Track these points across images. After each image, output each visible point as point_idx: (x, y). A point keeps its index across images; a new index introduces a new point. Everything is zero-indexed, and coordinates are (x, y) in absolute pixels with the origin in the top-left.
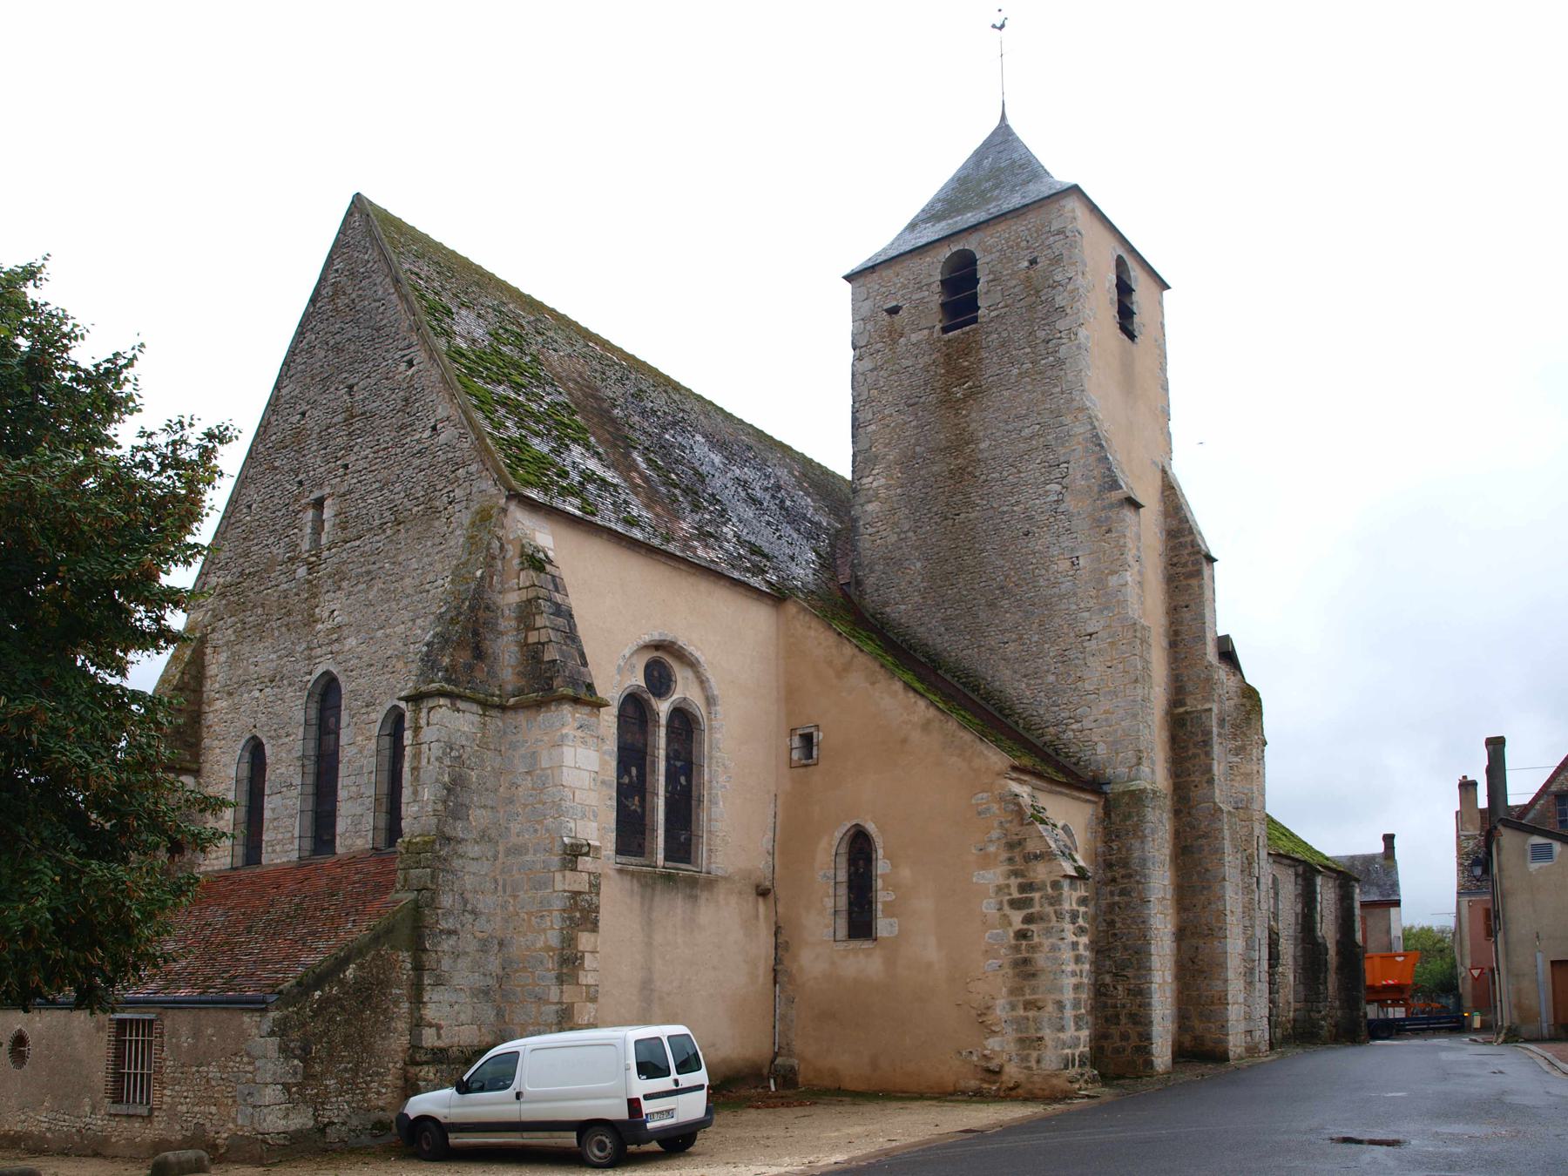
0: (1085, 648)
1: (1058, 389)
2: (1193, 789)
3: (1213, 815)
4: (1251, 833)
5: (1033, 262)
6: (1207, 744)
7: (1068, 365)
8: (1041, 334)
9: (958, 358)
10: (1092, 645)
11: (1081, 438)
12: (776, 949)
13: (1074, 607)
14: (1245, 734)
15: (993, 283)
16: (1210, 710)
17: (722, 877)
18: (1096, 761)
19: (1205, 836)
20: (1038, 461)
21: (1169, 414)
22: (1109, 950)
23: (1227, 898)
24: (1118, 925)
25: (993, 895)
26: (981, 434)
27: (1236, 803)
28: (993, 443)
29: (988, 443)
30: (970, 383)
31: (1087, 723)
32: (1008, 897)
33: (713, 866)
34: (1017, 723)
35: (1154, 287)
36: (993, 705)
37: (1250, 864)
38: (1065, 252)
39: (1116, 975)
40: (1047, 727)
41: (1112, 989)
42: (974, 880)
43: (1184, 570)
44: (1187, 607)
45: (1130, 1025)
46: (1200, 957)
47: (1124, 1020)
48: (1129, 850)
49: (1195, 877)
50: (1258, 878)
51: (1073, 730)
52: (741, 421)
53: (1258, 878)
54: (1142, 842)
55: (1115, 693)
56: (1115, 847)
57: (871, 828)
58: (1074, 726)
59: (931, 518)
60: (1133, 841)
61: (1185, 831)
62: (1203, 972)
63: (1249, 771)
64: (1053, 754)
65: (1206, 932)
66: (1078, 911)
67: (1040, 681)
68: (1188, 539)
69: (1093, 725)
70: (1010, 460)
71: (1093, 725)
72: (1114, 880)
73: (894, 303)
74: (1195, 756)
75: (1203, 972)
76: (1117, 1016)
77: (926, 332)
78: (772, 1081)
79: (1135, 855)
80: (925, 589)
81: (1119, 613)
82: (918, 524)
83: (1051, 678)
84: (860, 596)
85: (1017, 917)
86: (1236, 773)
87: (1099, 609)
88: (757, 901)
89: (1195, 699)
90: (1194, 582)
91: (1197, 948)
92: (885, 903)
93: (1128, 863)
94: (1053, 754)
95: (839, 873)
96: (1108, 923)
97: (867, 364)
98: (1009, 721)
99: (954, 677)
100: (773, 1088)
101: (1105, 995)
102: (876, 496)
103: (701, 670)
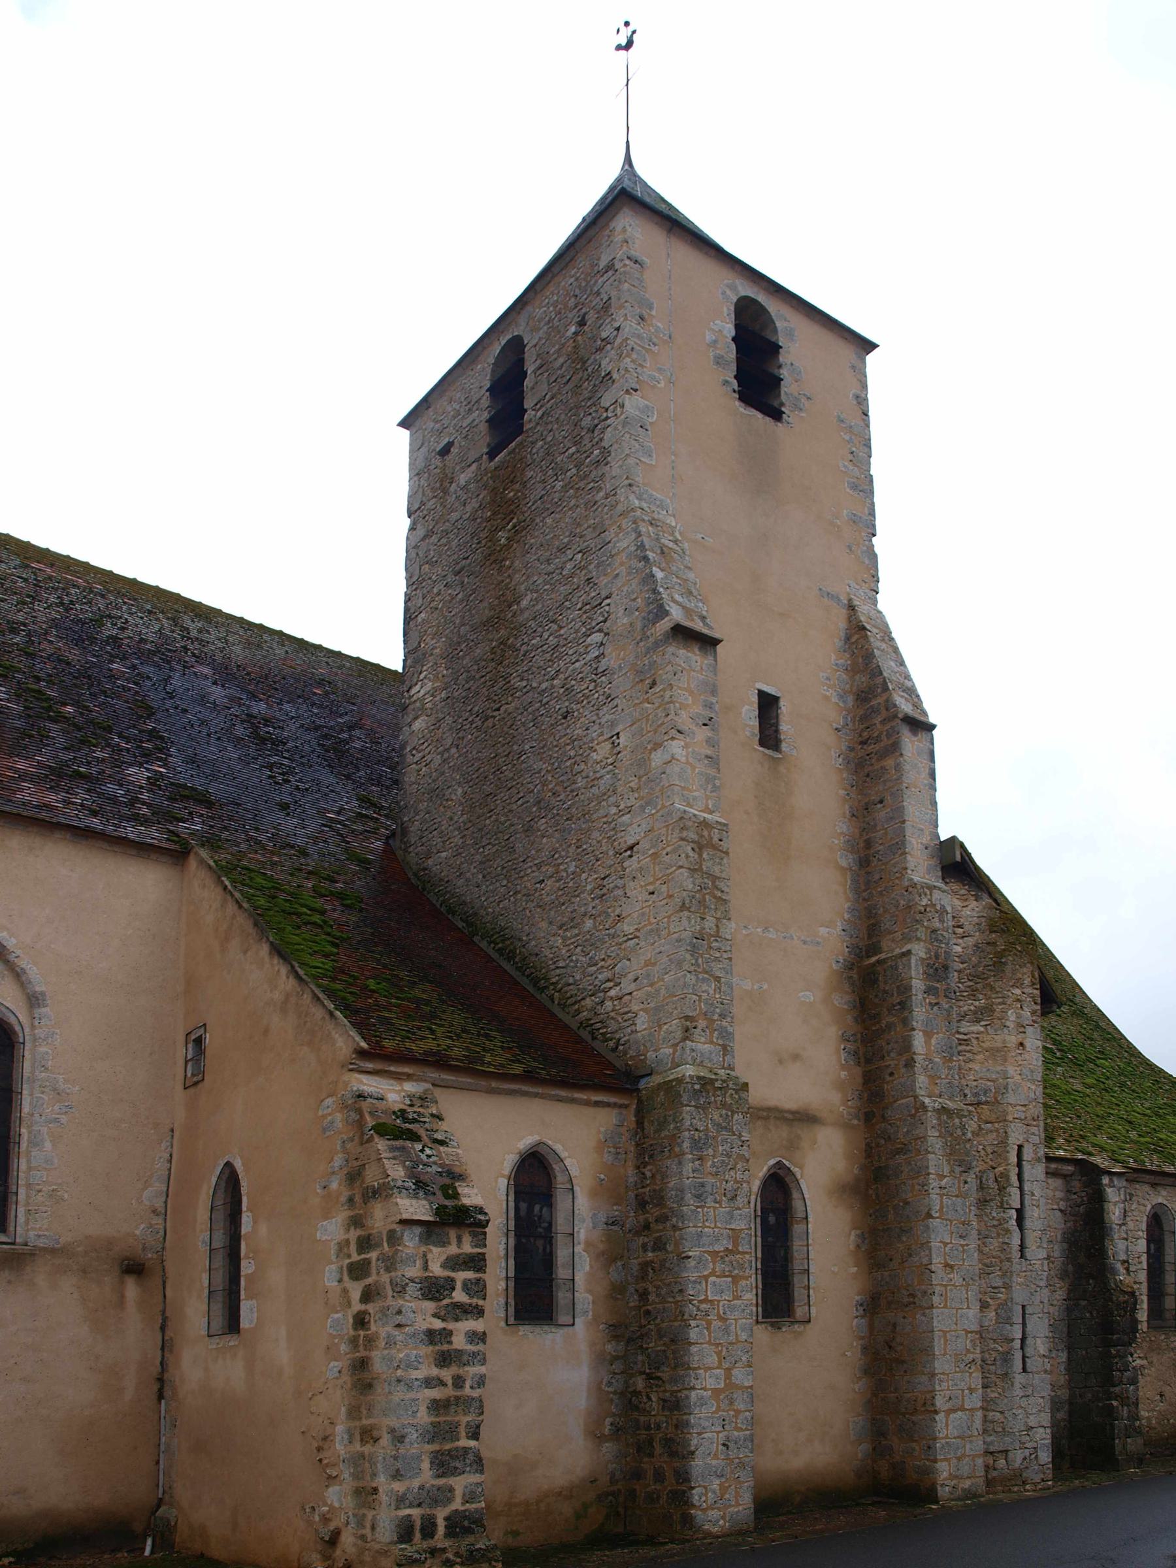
0: (624, 869)
1: (602, 494)
2: (888, 1078)
3: (913, 1116)
4: (1004, 1143)
5: (582, 323)
6: (904, 1005)
7: (613, 454)
8: (587, 422)
9: (505, 490)
10: (632, 864)
11: (624, 555)
12: (163, 1349)
13: (614, 810)
14: (992, 988)
15: (540, 372)
16: (909, 952)
17: (44, 1249)
18: (637, 1042)
19: (904, 1149)
20: (579, 606)
21: (874, 526)
22: (642, 1336)
23: (935, 1244)
24: (652, 1298)
25: (333, 1258)
26: (523, 587)
27: (976, 1095)
28: (535, 595)
29: (529, 598)
30: (515, 521)
31: (627, 985)
32: (348, 1261)
33: (32, 1234)
34: (552, 999)
35: (846, 351)
36: (528, 976)
37: (1002, 1189)
38: (614, 294)
39: (649, 1377)
40: (583, 999)
41: (645, 1399)
42: (318, 1235)
43: (877, 747)
44: (881, 802)
45: (665, 1458)
46: (898, 1340)
47: (658, 1449)
48: (664, 1176)
49: (891, 1217)
50: (1020, 1212)
51: (611, 998)
52: (319, 648)
53: (1020, 1212)
54: (680, 1163)
55: (657, 932)
56: (648, 1174)
57: (238, 1165)
58: (612, 993)
59: (472, 723)
60: (669, 1162)
61: (878, 1145)
62: (903, 1362)
63: (1000, 1045)
64: (589, 1038)
65: (906, 1300)
66: (453, 1280)
67: (576, 931)
68: (880, 700)
69: (633, 986)
70: (551, 613)
71: (633, 986)
72: (647, 1227)
73: (446, 440)
74: (889, 1027)
75: (903, 1362)
76: (650, 1442)
77: (474, 466)
78: (149, 1542)
79: (671, 1185)
80: (465, 824)
81: (663, 806)
82: (460, 735)
83: (589, 923)
84: (405, 850)
85: (356, 1290)
86: (975, 1049)
87: (641, 806)
88: (122, 1282)
89: (893, 941)
90: (889, 762)
91: (895, 1325)
92: (246, 1276)
93: (662, 1198)
94: (589, 1038)
95: (215, 1237)
96: (640, 1296)
97: (421, 532)
98: (543, 998)
99: (490, 943)
100: (147, 1552)
101: (637, 1408)
102: (423, 708)
103: (11, 957)
